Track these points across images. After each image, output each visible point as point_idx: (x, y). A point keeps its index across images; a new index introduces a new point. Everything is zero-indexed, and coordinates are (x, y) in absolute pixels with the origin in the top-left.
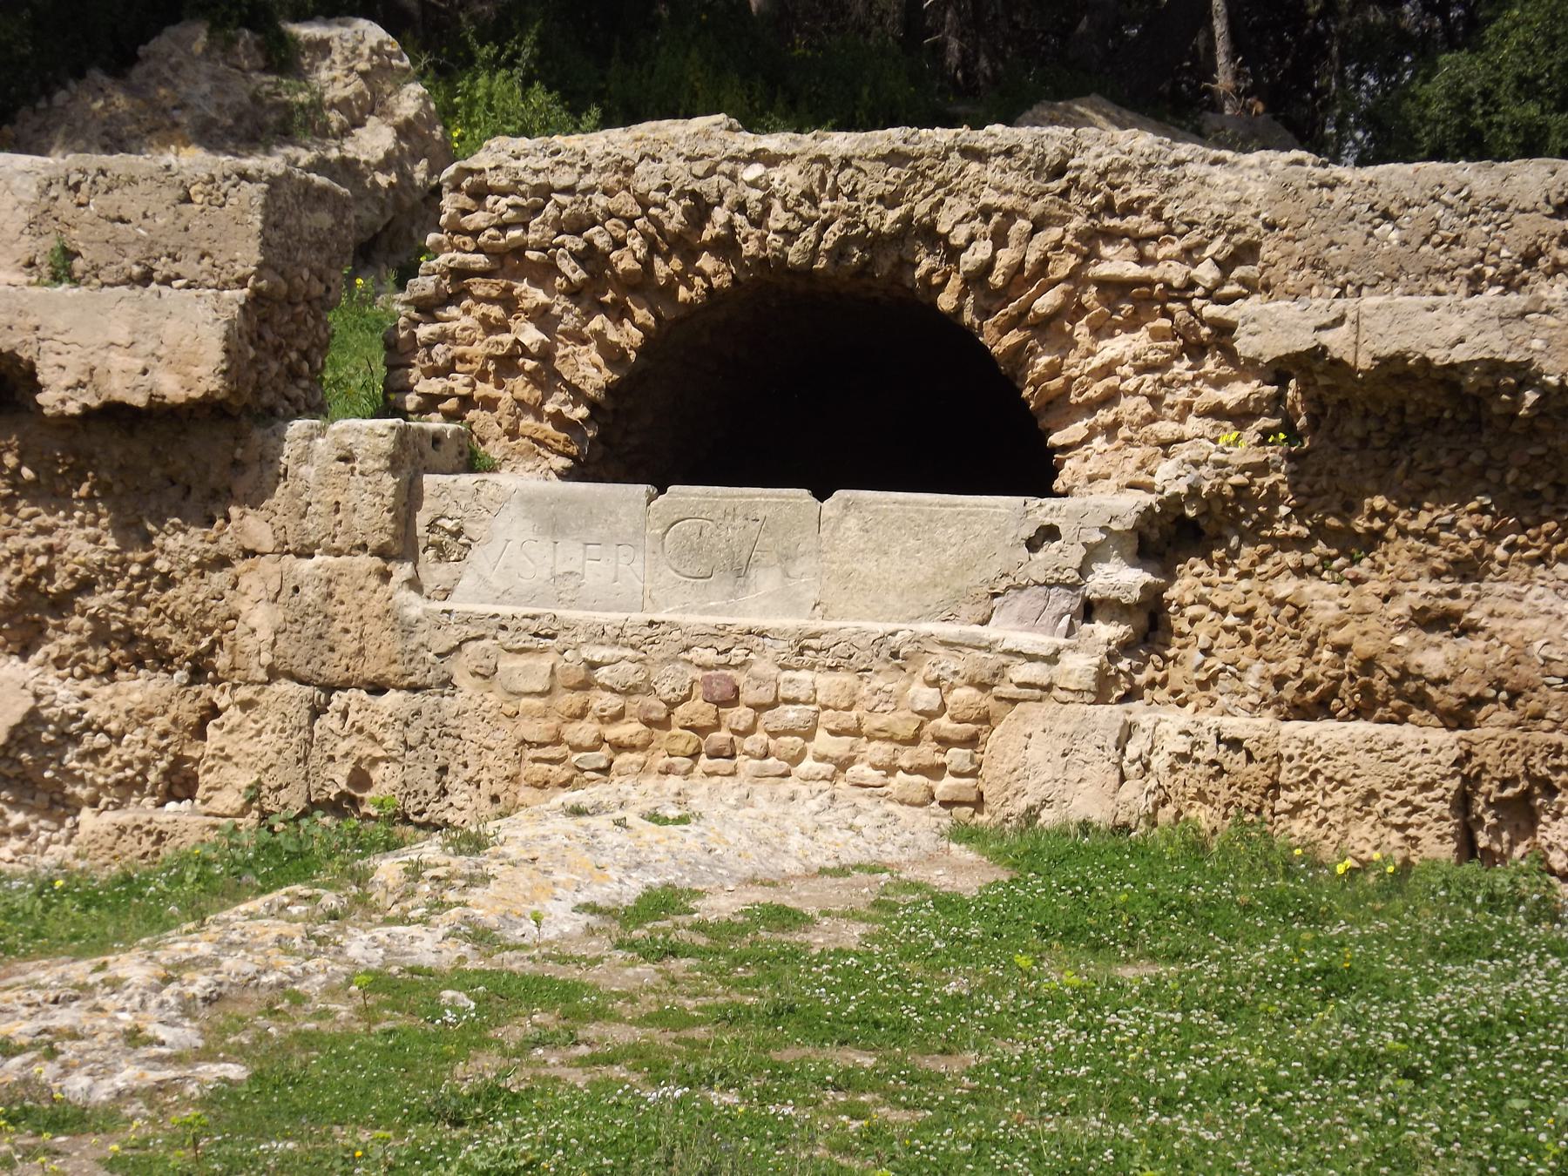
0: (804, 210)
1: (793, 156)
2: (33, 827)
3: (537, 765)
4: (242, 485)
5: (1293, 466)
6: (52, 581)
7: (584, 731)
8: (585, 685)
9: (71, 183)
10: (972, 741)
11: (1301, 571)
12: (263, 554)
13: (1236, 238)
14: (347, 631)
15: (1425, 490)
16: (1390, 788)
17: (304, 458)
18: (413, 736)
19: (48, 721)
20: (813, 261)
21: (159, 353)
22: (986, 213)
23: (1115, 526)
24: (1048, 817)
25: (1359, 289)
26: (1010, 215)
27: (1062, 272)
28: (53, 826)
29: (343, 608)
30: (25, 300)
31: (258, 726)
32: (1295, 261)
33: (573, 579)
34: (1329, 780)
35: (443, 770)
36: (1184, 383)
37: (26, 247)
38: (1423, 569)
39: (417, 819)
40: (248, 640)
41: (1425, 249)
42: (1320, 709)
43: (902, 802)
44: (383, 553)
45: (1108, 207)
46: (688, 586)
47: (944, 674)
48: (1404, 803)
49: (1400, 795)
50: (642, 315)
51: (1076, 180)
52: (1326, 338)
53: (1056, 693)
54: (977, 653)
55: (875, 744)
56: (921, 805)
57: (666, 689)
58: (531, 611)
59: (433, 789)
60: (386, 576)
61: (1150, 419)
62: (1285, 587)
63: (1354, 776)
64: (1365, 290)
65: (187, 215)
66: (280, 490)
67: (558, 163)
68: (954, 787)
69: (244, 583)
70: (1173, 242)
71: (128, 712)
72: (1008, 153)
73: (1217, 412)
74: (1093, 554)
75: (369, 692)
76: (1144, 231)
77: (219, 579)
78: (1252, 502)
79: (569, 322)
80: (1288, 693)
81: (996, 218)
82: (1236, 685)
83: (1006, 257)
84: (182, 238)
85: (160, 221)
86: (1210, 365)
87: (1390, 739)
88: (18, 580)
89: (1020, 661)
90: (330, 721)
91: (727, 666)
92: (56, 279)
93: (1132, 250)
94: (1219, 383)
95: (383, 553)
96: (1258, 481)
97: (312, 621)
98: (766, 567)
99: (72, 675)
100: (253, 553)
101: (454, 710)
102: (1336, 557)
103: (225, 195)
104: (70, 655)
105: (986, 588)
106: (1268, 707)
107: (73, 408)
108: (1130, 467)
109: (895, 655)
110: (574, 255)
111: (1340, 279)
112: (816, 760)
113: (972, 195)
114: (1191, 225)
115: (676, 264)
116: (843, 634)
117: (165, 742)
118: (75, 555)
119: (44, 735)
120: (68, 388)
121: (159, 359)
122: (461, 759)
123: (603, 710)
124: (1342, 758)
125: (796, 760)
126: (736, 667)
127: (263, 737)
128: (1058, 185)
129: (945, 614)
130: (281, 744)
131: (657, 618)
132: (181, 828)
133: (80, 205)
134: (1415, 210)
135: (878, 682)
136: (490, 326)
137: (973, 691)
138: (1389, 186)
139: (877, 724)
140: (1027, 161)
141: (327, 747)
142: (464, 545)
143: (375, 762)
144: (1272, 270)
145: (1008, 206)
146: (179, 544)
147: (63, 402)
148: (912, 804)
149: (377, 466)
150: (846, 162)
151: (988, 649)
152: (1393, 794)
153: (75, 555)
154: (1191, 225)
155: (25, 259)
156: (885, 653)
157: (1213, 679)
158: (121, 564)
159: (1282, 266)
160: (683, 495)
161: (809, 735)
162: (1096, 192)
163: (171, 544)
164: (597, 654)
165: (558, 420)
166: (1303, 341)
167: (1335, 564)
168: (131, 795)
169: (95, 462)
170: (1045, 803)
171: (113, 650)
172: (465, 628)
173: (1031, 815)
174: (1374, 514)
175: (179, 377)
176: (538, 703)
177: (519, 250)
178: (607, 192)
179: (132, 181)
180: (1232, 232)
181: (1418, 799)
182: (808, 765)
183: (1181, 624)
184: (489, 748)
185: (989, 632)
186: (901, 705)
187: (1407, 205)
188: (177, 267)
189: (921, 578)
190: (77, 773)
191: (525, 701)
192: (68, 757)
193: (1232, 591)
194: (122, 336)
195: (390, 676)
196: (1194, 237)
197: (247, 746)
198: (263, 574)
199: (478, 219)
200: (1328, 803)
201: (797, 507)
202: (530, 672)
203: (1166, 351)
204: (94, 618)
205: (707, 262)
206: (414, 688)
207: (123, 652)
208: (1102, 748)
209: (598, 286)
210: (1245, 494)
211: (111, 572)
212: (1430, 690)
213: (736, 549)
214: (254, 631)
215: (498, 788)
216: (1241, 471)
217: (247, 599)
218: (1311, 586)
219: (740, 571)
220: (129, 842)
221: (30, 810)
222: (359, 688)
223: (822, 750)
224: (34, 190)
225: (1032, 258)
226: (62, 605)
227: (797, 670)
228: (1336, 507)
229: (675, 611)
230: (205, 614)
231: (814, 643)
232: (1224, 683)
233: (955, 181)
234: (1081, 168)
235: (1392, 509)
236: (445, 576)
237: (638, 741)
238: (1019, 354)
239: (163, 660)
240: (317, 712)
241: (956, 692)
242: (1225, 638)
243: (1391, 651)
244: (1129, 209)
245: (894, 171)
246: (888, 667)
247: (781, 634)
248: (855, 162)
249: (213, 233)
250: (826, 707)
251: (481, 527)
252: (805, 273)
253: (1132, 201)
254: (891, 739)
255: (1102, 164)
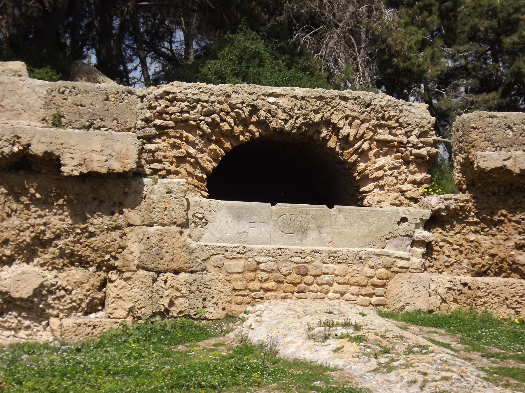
0: (291, 113)
1: (286, 95)
2: (32, 325)
3: (239, 297)
4: (129, 200)
5: (475, 200)
6: (45, 235)
7: (256, 285)
8: (255, 270)
9: (61, 91)
10: (384, 286)
11: (476, 232)
12: (135, 226)
13: (421, 129)
14: (167, 252)
15: (517, 208)
16: (511, 297)
17: (151, 192)
18: (193, 289)
19: (46, 286)
20: (292, 130)
21: (112, 154)
22: (347, 117)
23: (424, 218)
24: (407, 308)
25: (501, 148)
26: (354, 118)
27: (368, 137)
28: (38, 325)
29: (166, 244)
30: (58, 133)
31: (131, 286)
32: (483, 139)
33: (245, 234)
34: (493, 295)
35: (204, 300)
36: (404, 173)
37: (42, 113)
38: (516, 232)
39: (194, 317)
40: (130, 256)
41: (521, 137)
42: (484, 274)
43: (361, 305)
44: (182, 226)
45: (383, 118)
46: (286, 236)
47: (376, 264)
48: (515, 301)
49: (515, 299)
50: (228, 145)
51: (373, 109)
52: (506, 163)
53: (410, 270)
54: (387, 258)
55: (353, 287)
56: (367, 306)
57: (284, 270)
58: (236, 245)
59: (201, 306)
60: (181, 233)
61: (396, 184)
62: (472, 237)
63: (501, 293)
64: (503, 149)
65: (109, 105)
66: (142, 203)
67: (201, 92)
68: (378, 300)
69: (129, 235)
70: (401, 130)
71: (75, 283)
72: (355, 99)
73: (414, 182)
74: (417, 226)
75: (174, 273)
76: (393, 125)
77: (115, 234)
78: (465, 210)
79: (200, 145)
80: (476, 269)
81: (350, 119)
82: (460, 267)
83: (353, 132)
84: (106, 113)
85: (98, 107)
86: (412, 167)
87: (512, 282)
88: (33, 235)
89: (399, 260)
90: (160, 283)
91: (305, 262)
92: (54, 124)
93: (388, 131)
94: (413, 173)
95: (182, 226)
96: (467, 205)
97: (154, 249)
98: (313, 230)
99: (48, 269)
100: (132, 225)
101: (209, 279)
102: (486, 228)
103: (123, 99)
104: (48, 262)
105: (385, 237)
106: (468, 273)
107: (76, 173)
108: (391, 198)
109: (360, 258)
110: (207, 123)
111: (496, 145)
112: (334, 292)
113: (343, 111)
114: (408, 124)
115: (241, 128)
116: (344, 252)
117: (89, 293)
118: (55, 225)
119: (44, 292)
120: (75, 166)
121: (112, 156)
122: (211, 296)
123: (262, 278)
124: (498, 288)
125: (327, 293)
126: (307, 263)
127: (133, 290)
128: (368, 110)
129: (372, 245)
130: (141, 292)
131: (281, 247)
132: (103, 323)
133: (64, 99)
134: (517, 126)
135: (355, 267)
136: (174, 146)
137: (385, 270)
138: (510, 118)
139: (355, 281)
140: (362, 102)
141: (160, 293)
142: (204, 222)
143: (177, 297)
144: (476, 142)
145: (354, 115)
146: (99, 221)
147: (72, 171)
148: (365, 306)
149: (181, 195)
150: (303, 98)
151: (390, 256)
152: (513, 298)
153: (55, 225)
154: (408, 124)
155: (42, 118)
156: (358, 258)
157: (452, 265)
158: (72, 229)
159: (479, 140)
160: (284, 206)
161: (331, 285)
162: (380, 112)
163: (95, 221)
164: (261, 259)
165: (201, 179)
166: (499, 164)
167: (486, 230)
168: (72, 312)
169: (68, 192)
170: (408, 304)
171: (64, 260)
172: (213, 251)
173: (403, 308)
174: (502, 215)
175: (121, 163)
176: (239, 276)
177: (187, 120)
178: (220, 103)
179: (86, 92)
180: (420, 128)
181: (519, 300)
182: (330, 294)
183: (436, 248)
184: (222, 292)
185: (389, 250)
186: (362, 274)
187: (515, 124)
188: (103, 123)
189: (364, 234)
190: (52, 305)
191: (234, 275)
192: (49, 299)
193: (454, 237)
194: (98, 148)
195: (184, 268)
196: (409, 128)
197: (128, 294)
198: (135, 235)
199: (171, 109)
200: (493, 302)
201: (324, 211)
202: (238, 265)
203: (400, 163)
204: (61, 248)
205: (252, 127)
206: (192, 272)
207: (67, 261)
208: (424, 287)
209: (216, 133)
210: (463, 209)
211: (69, 232)
212: (520, 267)
213: (303, 224)
214: (132, 252)
215: (225, 305)
216: (463, 202)
217: (130, 241)
218: (479, 236)
219: (304, 231)
220: (80, 330)
221: (31, 319)
222: (170, 272)
223: (337, 289)
224: (45, 92)
225: (361, 132)
226: (46, 244)
227: (328, 263)
228: (489, 213)
229: (282, 244)
230: (109, 246)
231: (334, 255)
232: (456, 266)
233: (337, 107)
234: (376, 105)
235: (507, 214)
236: (198, 233)
237: (274, 288)
238: (355, 163)
239: (84, 263)
240: (154, 280)
241: (379, 270)
242: (453, 253)
243: (510, 256)
244: (389, 119)
245: (319, 102)
246: (358, 262)
247: (324, 252)
248: (306, 99)
249: (119, 112)
250: (337, 276)
251: (212, 216)
252: (289, 133)
253: (390, 116)
254: (358, 285)
255: (383, 104)
